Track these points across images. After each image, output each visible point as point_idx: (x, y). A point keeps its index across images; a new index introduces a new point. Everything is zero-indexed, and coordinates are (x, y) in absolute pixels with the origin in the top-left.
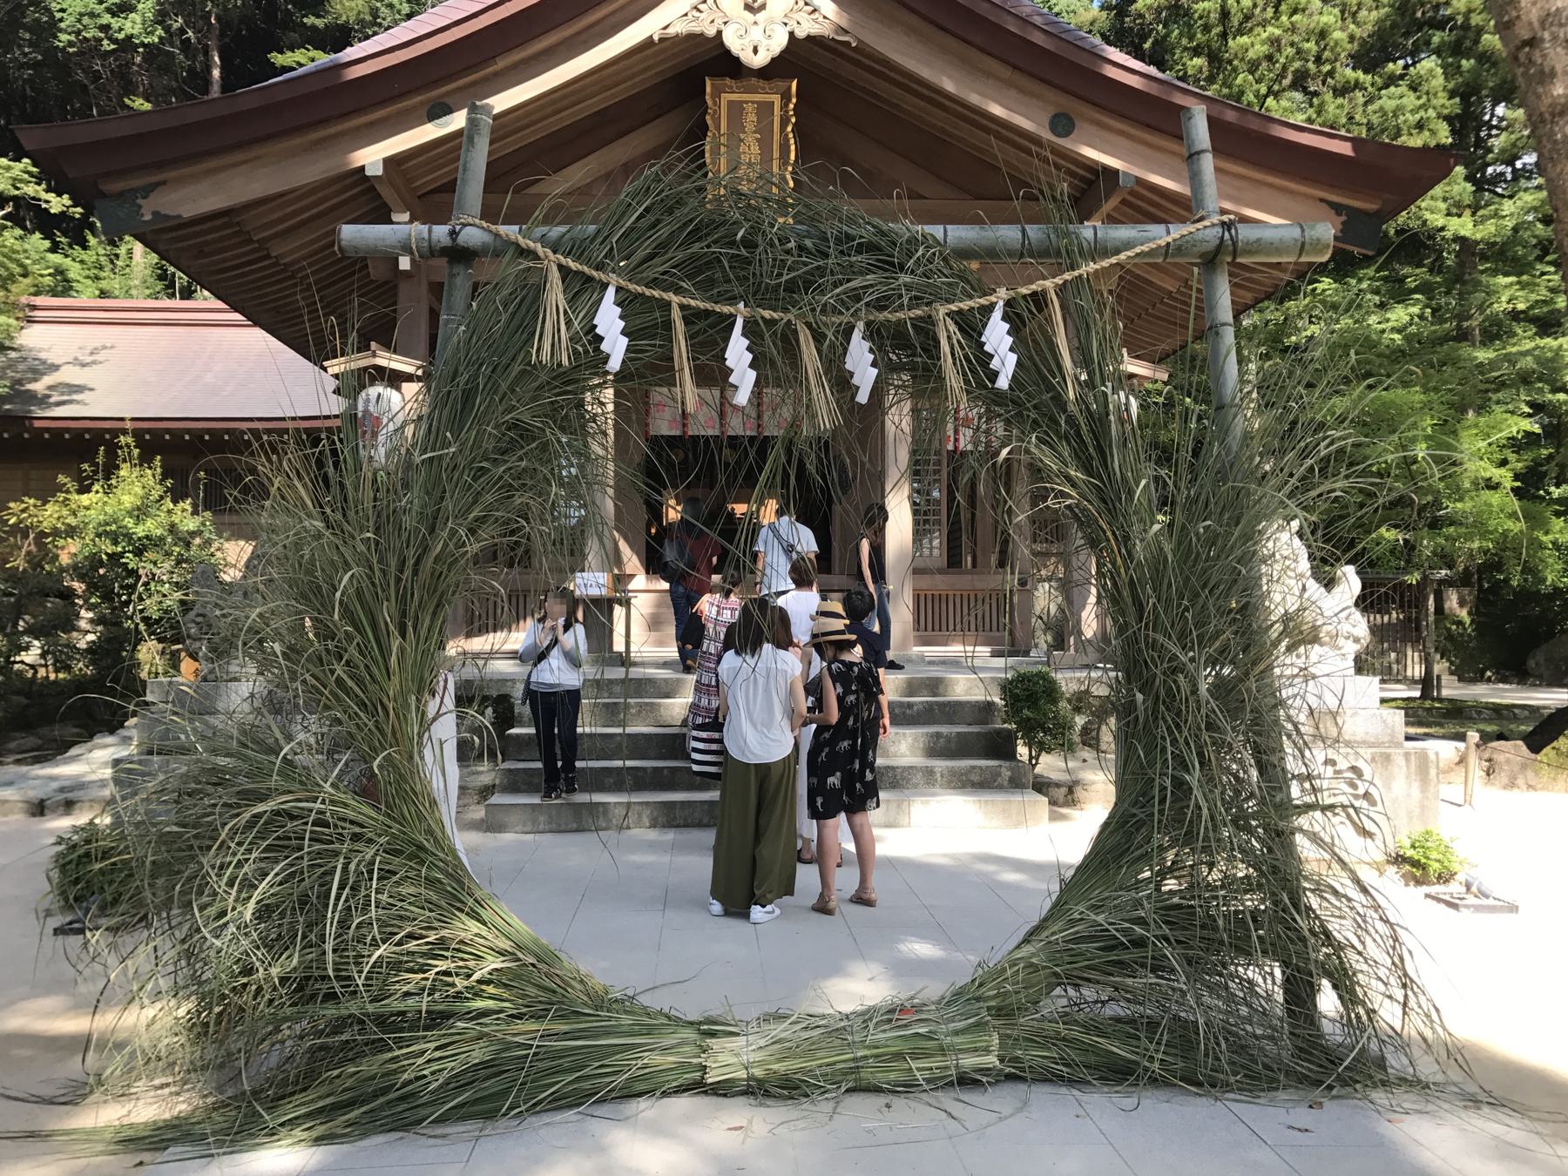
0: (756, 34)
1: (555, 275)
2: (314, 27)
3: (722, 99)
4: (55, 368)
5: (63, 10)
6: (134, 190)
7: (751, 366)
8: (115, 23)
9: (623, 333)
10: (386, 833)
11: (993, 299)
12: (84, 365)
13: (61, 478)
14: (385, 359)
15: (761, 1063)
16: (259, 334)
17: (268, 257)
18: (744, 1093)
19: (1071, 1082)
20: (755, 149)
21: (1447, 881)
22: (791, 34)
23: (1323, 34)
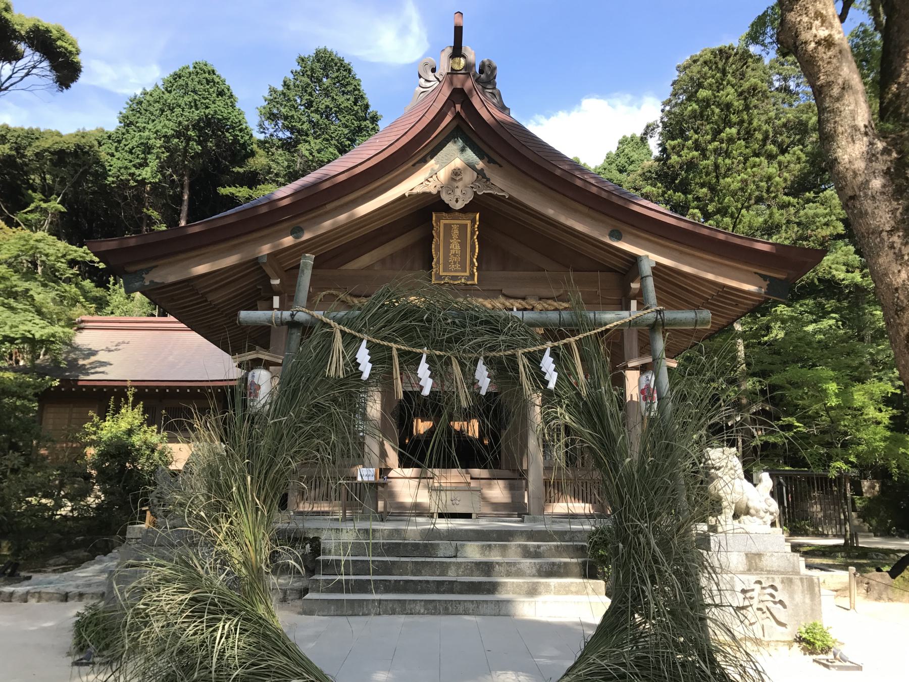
1: (338, 336)
2: (238, 173)
3: (440, 223)
6: (142, 270)
7: (430, 377)
8: (137, 172)
9: (369, 362)
10: (244, 610)
11: (545, 346)
12: (110, 351)
13: (91, 413)
14: (264, 356)
16: (194, 333)
17: (206, 301)
20: (458, 247)
21: (826, 653)
22: (475, 192)
23: (770, 178)
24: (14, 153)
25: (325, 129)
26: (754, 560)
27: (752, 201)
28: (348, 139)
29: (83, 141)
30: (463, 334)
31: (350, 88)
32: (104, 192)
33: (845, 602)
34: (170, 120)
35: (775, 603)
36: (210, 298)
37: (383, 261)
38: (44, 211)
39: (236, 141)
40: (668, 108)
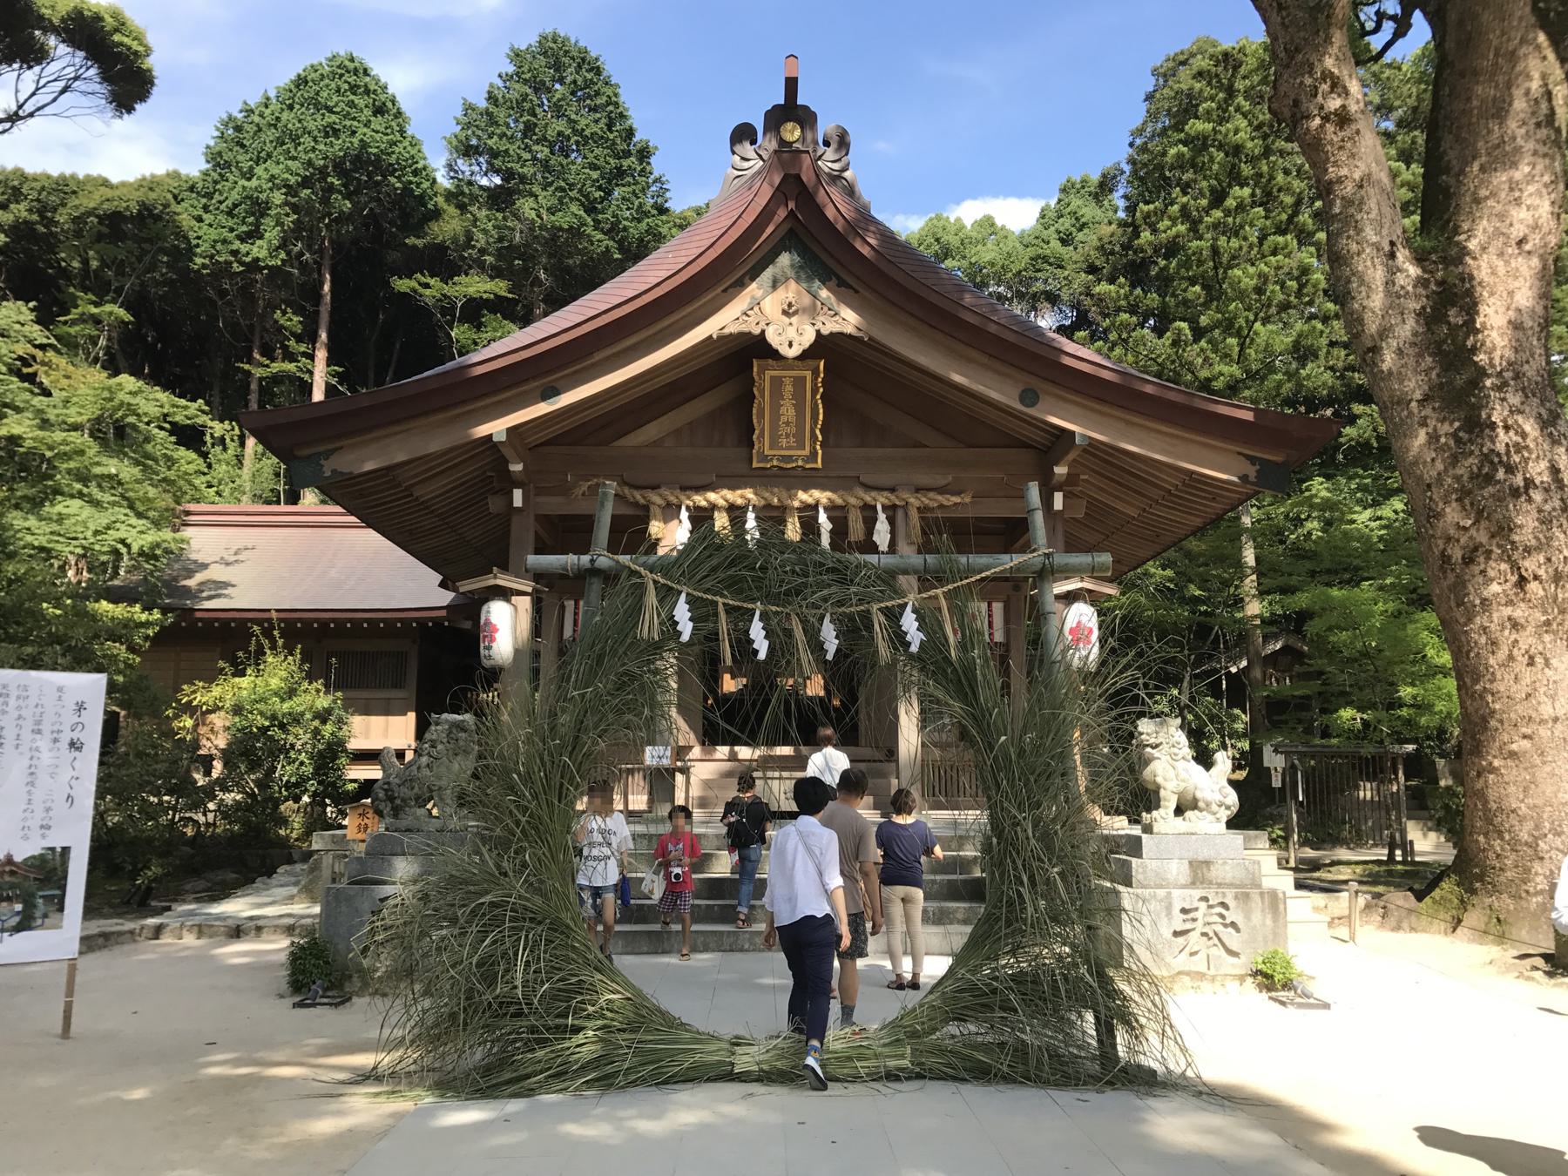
0: (791, 333)
1: (651, 586)
2: (415, 247)
3: (764, 376)
4: (205, 566)
5: (199, 238)
8: (244, 248)
12: (228, 564)
13: (221, 664)
14: (503, 581)
15: (766, 1062)
16: (372, 536)
18: (757, 1081)
19: (955, 1079)
20: (792, 412)
22: (818, 332)
24: (35, 217)
25: (561, 173)
26: (1199, 871)
27: (1273, 310)
28: (600, 188)
29: (153, 195)
30: (805, 585)
31: (601, 100)
32: (190, 280)
33: (1343, 932)
34: (294, 158)
35: (1225, 926)
36: (418, 492)
37: (677, 433)
38: (96, 321)
39: (407, 189)
40: (1138, 142)
